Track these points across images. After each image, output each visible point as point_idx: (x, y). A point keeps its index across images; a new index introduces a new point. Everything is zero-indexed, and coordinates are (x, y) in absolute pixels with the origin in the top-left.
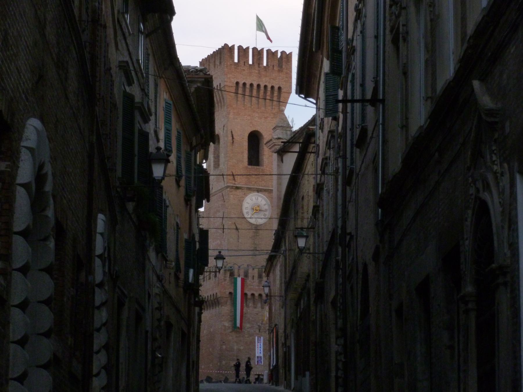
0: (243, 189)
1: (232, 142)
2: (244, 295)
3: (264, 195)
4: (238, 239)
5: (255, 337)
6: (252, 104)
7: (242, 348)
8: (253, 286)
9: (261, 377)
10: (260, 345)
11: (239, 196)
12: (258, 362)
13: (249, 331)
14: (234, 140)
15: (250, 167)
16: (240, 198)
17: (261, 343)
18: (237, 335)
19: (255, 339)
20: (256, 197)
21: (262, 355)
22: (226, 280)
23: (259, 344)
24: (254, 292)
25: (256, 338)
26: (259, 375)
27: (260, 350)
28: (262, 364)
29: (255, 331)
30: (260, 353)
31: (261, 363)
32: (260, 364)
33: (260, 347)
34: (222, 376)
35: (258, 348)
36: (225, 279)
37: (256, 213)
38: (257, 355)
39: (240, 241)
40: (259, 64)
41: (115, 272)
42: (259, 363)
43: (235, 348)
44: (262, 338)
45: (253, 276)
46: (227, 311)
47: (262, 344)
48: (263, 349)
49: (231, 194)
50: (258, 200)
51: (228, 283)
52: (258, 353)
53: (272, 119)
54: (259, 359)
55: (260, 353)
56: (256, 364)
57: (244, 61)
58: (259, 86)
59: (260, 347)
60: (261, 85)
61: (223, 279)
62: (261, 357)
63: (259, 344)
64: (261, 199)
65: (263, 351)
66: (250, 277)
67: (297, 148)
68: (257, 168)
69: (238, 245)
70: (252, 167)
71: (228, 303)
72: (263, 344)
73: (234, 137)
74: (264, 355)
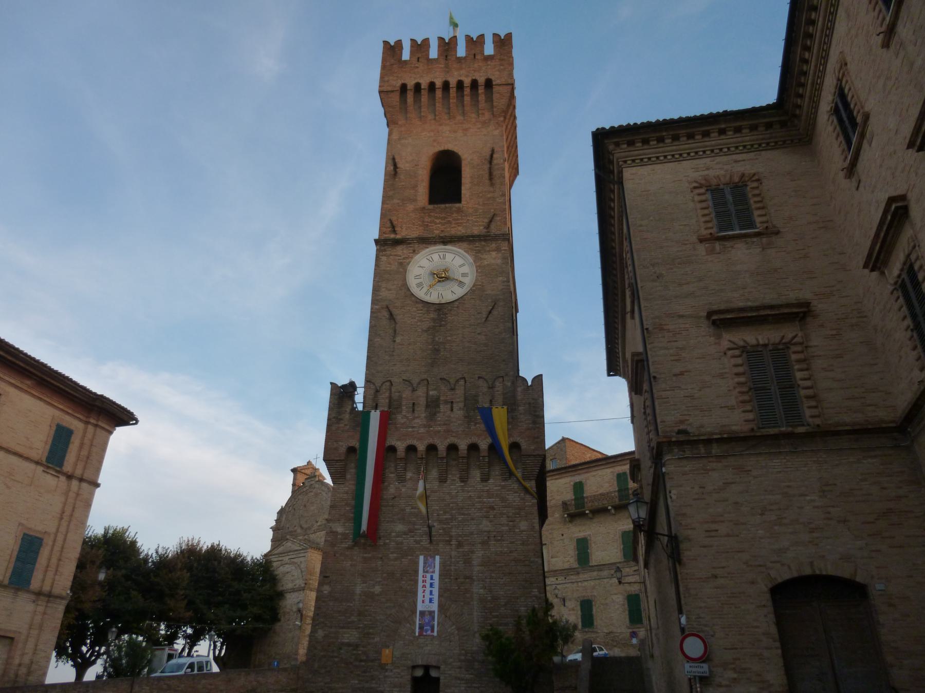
0: (410, 243)
1: (393, 173)
2: (386, 451)
3: (460, 248)
4: (394, 337)
5: (418, 557)
6: (437, 113)
7: (377, 589)
8: (413, 427)
9: (434, 673)
10: (432, 578)
11: (400, 256)
12: (421, 628)
13: (402, 543)
14: (398, 170)
15: (431, 207)
16: (404, 259)
17: (433, 572)
18: (365, 555)
19: (417, 563)
20: (441, 254)
21: (435, 607)
22: (341, 419)
23: (428, 575)
24: (415, 443)
25: (421, 558)
26: (427, 668)
27: (431, 593)
28: (435, 634)
29: (417, 542)
30: (431, 601)
31: (433, 631)
32: (429, 633)
33: (431, 585)
34: (310, 676)
35: (424, 586)
36: (339, 417)
37: (438, 284)
38: (420, 607)
39: (398, 339)
40: (446, 56)
41: (521, 501)
42: (426, 631)
43: (358, 590)
44: (437, 558)
45: (414, 404)
46: (345, 496)
47: (436, 576)
48: (440, 588)
49: (382, 256)
50: (444, 257)
51: (346, 425)
52: (423, 602)
53: (478, 130)
54: (427, 618)
55: (431, 601)
56: (417, 634)
57: (417, 57)
58: (446, 85)
59: (431, 585)
60: (451, 83)
61: (334, 418)
62: (431, 613)
63: (428, 575)
64: (453, 256)
65: (440, 596)
66: (404, 408)
67: (735, 346)
68: (446, 207)
69: (394, 348)
70: (436, 206)
71: (348, 476)
72: (440, 575)
73: (398, 165)
74: (440, 606)
